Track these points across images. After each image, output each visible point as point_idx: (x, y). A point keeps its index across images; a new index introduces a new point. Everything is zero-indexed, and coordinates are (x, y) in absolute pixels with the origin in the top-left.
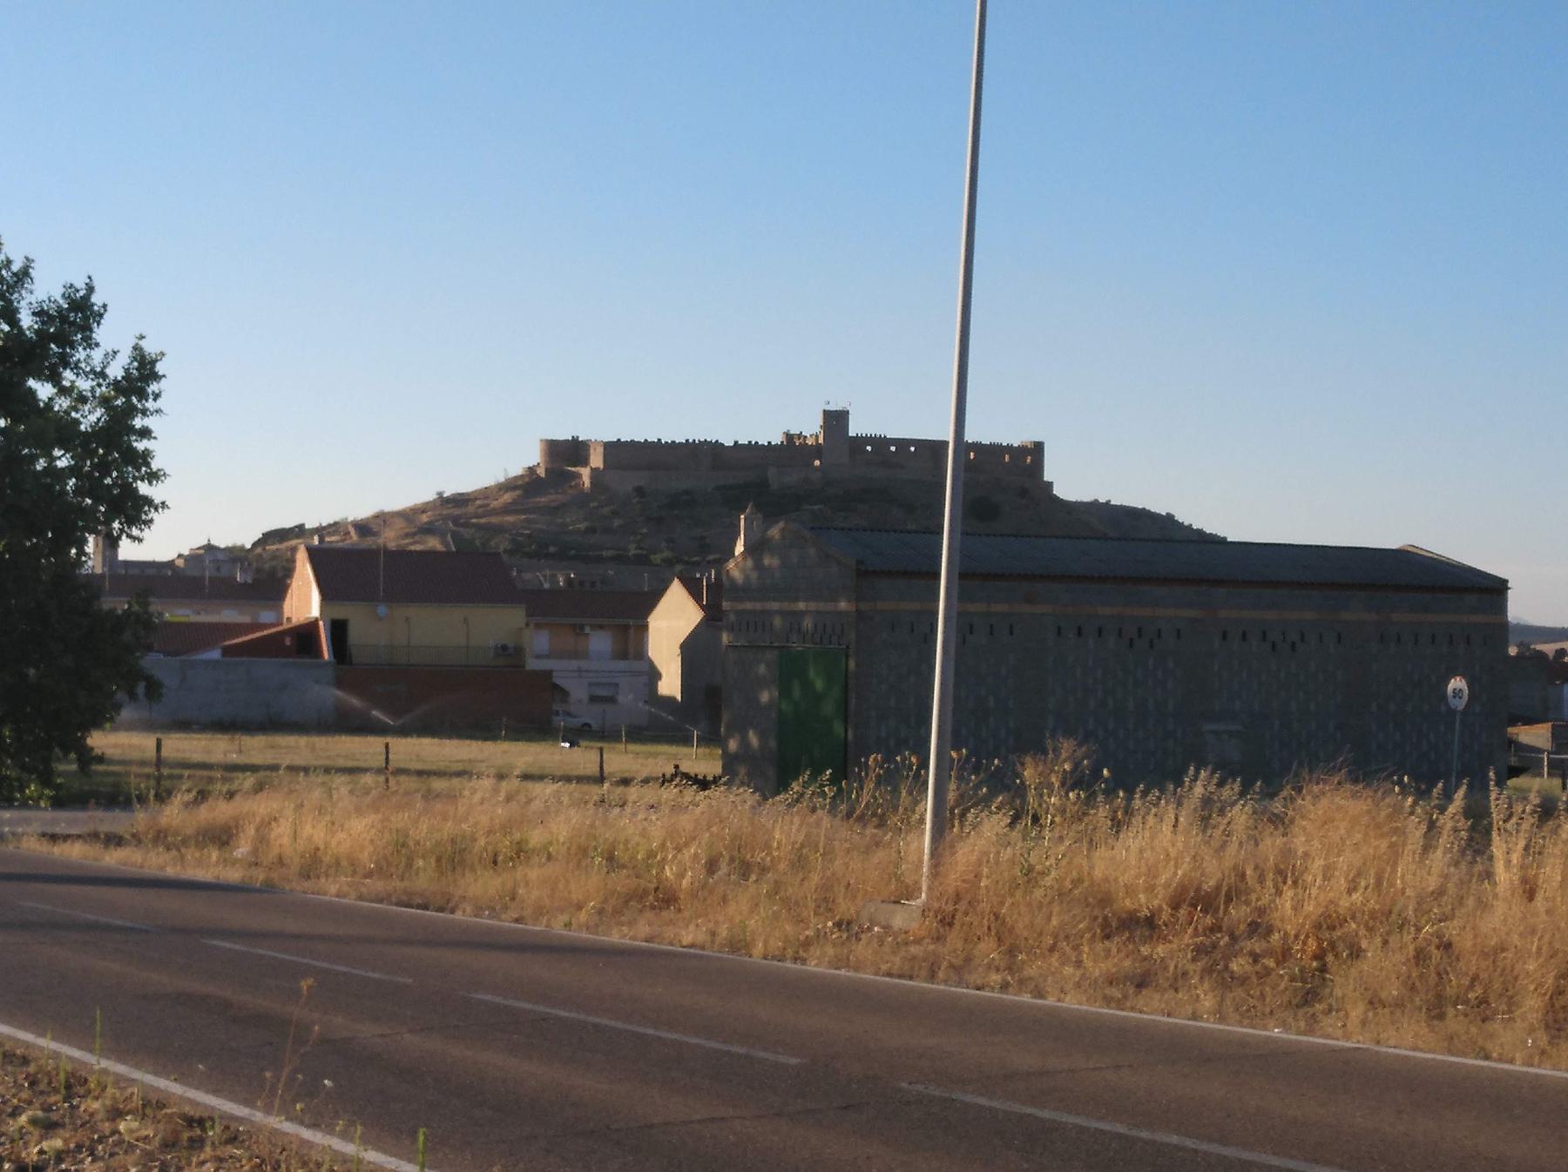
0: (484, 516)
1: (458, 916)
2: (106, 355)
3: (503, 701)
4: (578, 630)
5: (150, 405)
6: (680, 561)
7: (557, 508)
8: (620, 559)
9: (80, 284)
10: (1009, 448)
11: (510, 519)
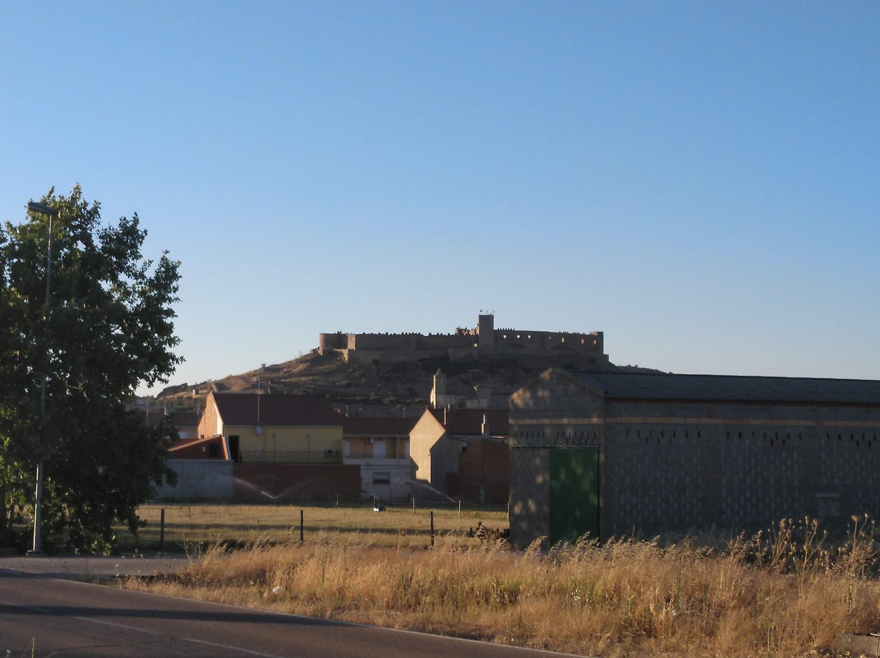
0: (287, 378)
1: (496, 643)
2: (145, 263)
3: (332, 483)
4: (367, 441)
5: (171, 295)
6: (399, 402)
7: (329, 373)
8: (365, 402)
9: (130, 218)
10: (584, 336)
11: (303, 379)
